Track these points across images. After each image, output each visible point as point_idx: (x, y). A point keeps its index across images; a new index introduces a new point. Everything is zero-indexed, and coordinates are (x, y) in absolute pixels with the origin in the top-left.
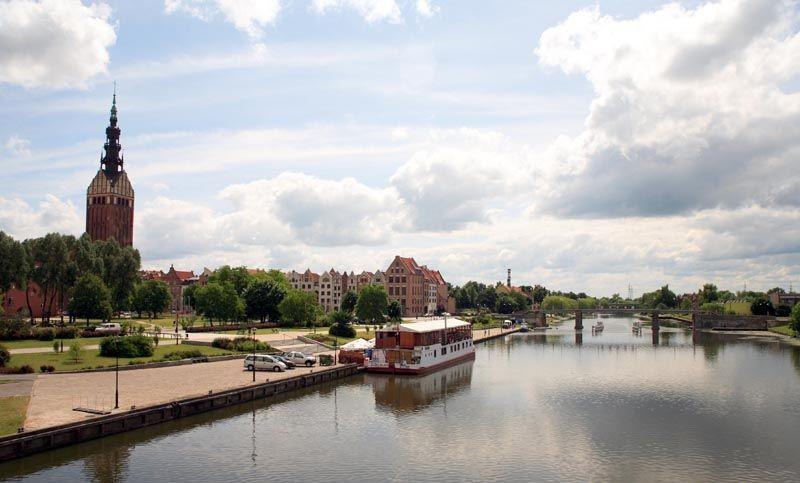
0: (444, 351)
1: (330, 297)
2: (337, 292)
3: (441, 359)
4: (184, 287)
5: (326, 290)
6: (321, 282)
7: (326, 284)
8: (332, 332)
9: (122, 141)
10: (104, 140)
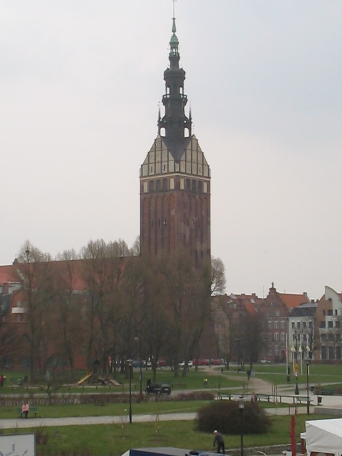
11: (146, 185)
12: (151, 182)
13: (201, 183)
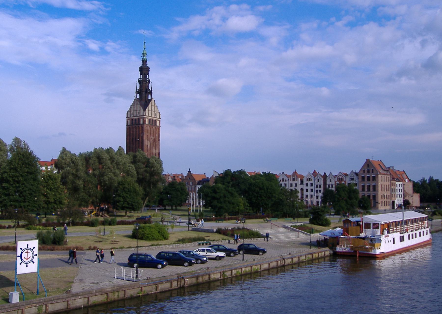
0: (402, 239)
1: (312, 193)
2: (318, 189)
3: (399, 245)
4: (199, 186)
5: (309, 188)
6: (305, 182)
7: (309, 183)
8: (312, 222)
9: (151, 76)
10: (137, 76)
11: (129, 121)
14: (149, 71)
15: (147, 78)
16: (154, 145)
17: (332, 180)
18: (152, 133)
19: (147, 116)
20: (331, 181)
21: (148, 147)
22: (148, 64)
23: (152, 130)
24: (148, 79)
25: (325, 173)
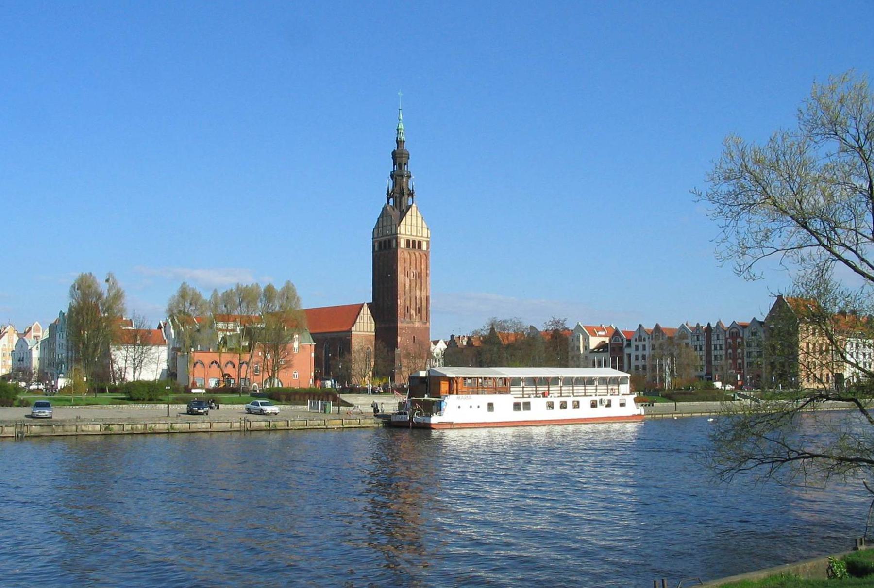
9: (412, 166)
11: (376, 244)
12: (380, 243)
13: (390, 241)
14: (409, 158)
15: (406, 169)
16: (419, 285)
17: (720, 336)
18: (413, 262)
19: (402, 234)
20: (718, 339)
21: (405, 288)
22: (407, 146)
23: (413, 257)
24: (407, 171)
25: (709, 324)
